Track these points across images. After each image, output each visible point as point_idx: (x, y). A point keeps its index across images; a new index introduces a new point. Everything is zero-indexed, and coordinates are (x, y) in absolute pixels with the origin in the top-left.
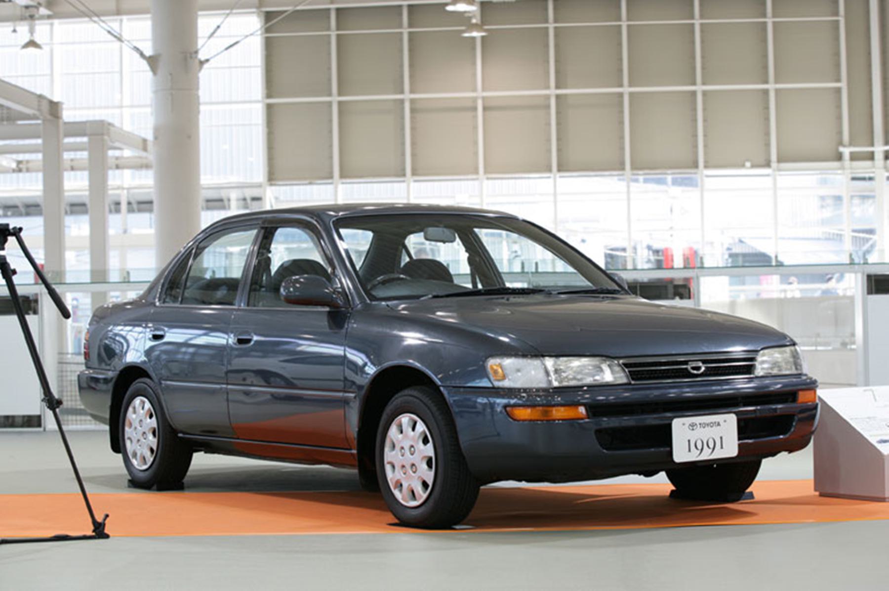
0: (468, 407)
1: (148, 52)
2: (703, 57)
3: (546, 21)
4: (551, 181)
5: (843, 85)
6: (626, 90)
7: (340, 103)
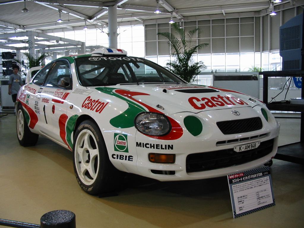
0: (258, 127)
1: (107, 33)
2: (226, 31)
3: (210, 24)
4: (210, 56)
5: (254, 36)
6: (225, 37)
7: (158, 41)
